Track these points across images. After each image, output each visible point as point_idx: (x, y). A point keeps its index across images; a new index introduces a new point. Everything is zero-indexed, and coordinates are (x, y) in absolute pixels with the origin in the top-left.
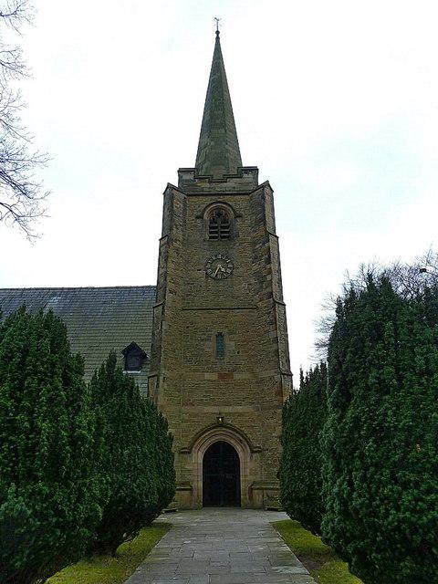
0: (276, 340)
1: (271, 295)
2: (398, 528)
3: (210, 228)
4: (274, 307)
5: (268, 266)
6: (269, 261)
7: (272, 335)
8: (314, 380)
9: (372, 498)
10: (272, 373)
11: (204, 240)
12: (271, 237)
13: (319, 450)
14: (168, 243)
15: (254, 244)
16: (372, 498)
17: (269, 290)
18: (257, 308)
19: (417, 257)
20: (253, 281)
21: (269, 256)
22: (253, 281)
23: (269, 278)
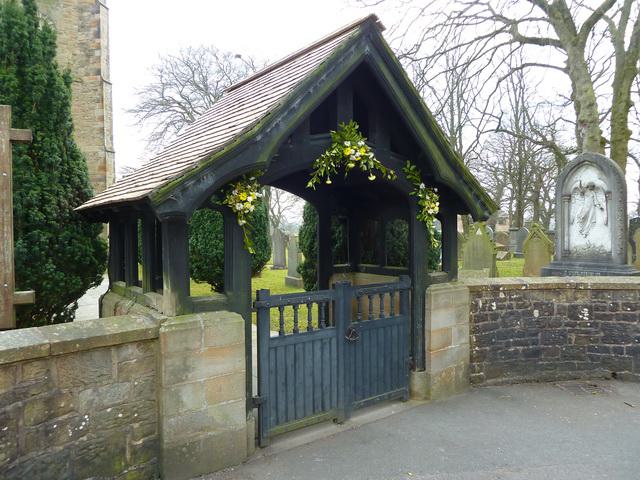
0: (102, 119)
1: (98, 72)
2: (216, 256)
4: (101, 84)
5: (97, 41)
6: (98, 35)
7: (97, 113)
8: (102, 273)
9: (206, 245)
10: (96, 149)
12: (102, 8)
13: (69, 179)
15: (82, 10)
16: (206, 245)
17: (96, 66)
18: (82, 82)
19: (190, 50)
20: (78, 52)
21: (99, 29)
22: (78, 52)
23: (97, 53)
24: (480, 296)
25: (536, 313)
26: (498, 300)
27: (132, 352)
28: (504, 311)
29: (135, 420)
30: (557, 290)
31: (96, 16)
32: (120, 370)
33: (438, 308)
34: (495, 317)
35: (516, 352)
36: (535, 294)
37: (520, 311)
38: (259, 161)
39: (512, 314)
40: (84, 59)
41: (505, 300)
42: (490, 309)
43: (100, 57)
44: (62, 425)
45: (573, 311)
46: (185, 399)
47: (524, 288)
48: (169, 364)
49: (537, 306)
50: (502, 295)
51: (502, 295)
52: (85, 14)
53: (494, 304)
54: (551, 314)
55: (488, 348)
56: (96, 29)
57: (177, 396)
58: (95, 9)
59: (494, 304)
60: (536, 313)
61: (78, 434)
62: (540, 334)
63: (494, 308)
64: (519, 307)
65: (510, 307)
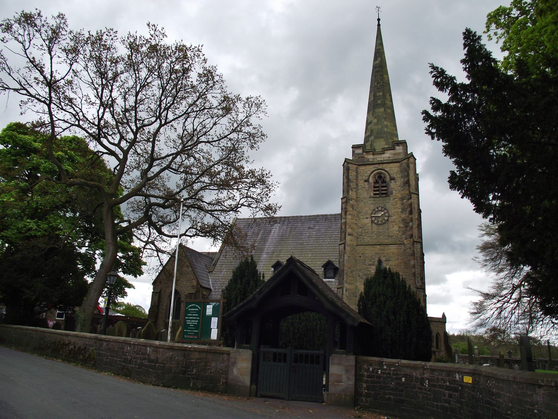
3: (375, 187)
5: (410, 216)
11: (370, 197)
14: (346, 202)
24: (371, 365)
25: (403, 379)
26: (382, 369)
27: (225, 355)
28: (385, 375)
29: (224, 374)
30: (415, 368)
31: (410, 201)
32: (222, 360)
33: (333, 364)
34: (379, 377)
35: (390, 398)
36: (405, 369)
37: (395, 377)
38: (147, 312)
39: (389, 378)
40: (404, 229)
41: (386, 370)
42: (377, 372)
43: (412, 227)
44: (208, 369)
45: (422, 380)
46: (234, 371)
47: (397, 364)
48: (232, 360)
49: (405, 375)
50: (385, 367)
51: (385, 367)
52: (405, 201)
53: (380, 371)
54: (412, 381)
55: (372, 392)
56: (409, 209)
57: (232, 370)
58: (409, 197)
59: (380, 371)
60: (403, 379)
61: (211, 373)
62: (404, 392)
63: (379, 373)
64: (394, 374)
65: (389, 374)
